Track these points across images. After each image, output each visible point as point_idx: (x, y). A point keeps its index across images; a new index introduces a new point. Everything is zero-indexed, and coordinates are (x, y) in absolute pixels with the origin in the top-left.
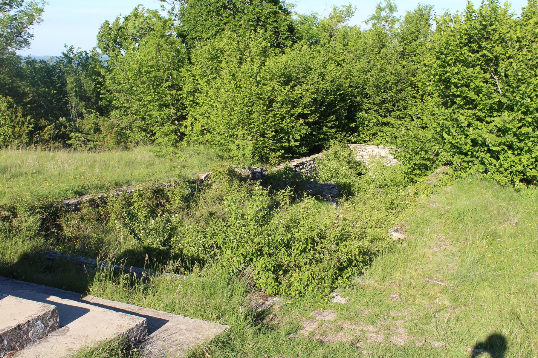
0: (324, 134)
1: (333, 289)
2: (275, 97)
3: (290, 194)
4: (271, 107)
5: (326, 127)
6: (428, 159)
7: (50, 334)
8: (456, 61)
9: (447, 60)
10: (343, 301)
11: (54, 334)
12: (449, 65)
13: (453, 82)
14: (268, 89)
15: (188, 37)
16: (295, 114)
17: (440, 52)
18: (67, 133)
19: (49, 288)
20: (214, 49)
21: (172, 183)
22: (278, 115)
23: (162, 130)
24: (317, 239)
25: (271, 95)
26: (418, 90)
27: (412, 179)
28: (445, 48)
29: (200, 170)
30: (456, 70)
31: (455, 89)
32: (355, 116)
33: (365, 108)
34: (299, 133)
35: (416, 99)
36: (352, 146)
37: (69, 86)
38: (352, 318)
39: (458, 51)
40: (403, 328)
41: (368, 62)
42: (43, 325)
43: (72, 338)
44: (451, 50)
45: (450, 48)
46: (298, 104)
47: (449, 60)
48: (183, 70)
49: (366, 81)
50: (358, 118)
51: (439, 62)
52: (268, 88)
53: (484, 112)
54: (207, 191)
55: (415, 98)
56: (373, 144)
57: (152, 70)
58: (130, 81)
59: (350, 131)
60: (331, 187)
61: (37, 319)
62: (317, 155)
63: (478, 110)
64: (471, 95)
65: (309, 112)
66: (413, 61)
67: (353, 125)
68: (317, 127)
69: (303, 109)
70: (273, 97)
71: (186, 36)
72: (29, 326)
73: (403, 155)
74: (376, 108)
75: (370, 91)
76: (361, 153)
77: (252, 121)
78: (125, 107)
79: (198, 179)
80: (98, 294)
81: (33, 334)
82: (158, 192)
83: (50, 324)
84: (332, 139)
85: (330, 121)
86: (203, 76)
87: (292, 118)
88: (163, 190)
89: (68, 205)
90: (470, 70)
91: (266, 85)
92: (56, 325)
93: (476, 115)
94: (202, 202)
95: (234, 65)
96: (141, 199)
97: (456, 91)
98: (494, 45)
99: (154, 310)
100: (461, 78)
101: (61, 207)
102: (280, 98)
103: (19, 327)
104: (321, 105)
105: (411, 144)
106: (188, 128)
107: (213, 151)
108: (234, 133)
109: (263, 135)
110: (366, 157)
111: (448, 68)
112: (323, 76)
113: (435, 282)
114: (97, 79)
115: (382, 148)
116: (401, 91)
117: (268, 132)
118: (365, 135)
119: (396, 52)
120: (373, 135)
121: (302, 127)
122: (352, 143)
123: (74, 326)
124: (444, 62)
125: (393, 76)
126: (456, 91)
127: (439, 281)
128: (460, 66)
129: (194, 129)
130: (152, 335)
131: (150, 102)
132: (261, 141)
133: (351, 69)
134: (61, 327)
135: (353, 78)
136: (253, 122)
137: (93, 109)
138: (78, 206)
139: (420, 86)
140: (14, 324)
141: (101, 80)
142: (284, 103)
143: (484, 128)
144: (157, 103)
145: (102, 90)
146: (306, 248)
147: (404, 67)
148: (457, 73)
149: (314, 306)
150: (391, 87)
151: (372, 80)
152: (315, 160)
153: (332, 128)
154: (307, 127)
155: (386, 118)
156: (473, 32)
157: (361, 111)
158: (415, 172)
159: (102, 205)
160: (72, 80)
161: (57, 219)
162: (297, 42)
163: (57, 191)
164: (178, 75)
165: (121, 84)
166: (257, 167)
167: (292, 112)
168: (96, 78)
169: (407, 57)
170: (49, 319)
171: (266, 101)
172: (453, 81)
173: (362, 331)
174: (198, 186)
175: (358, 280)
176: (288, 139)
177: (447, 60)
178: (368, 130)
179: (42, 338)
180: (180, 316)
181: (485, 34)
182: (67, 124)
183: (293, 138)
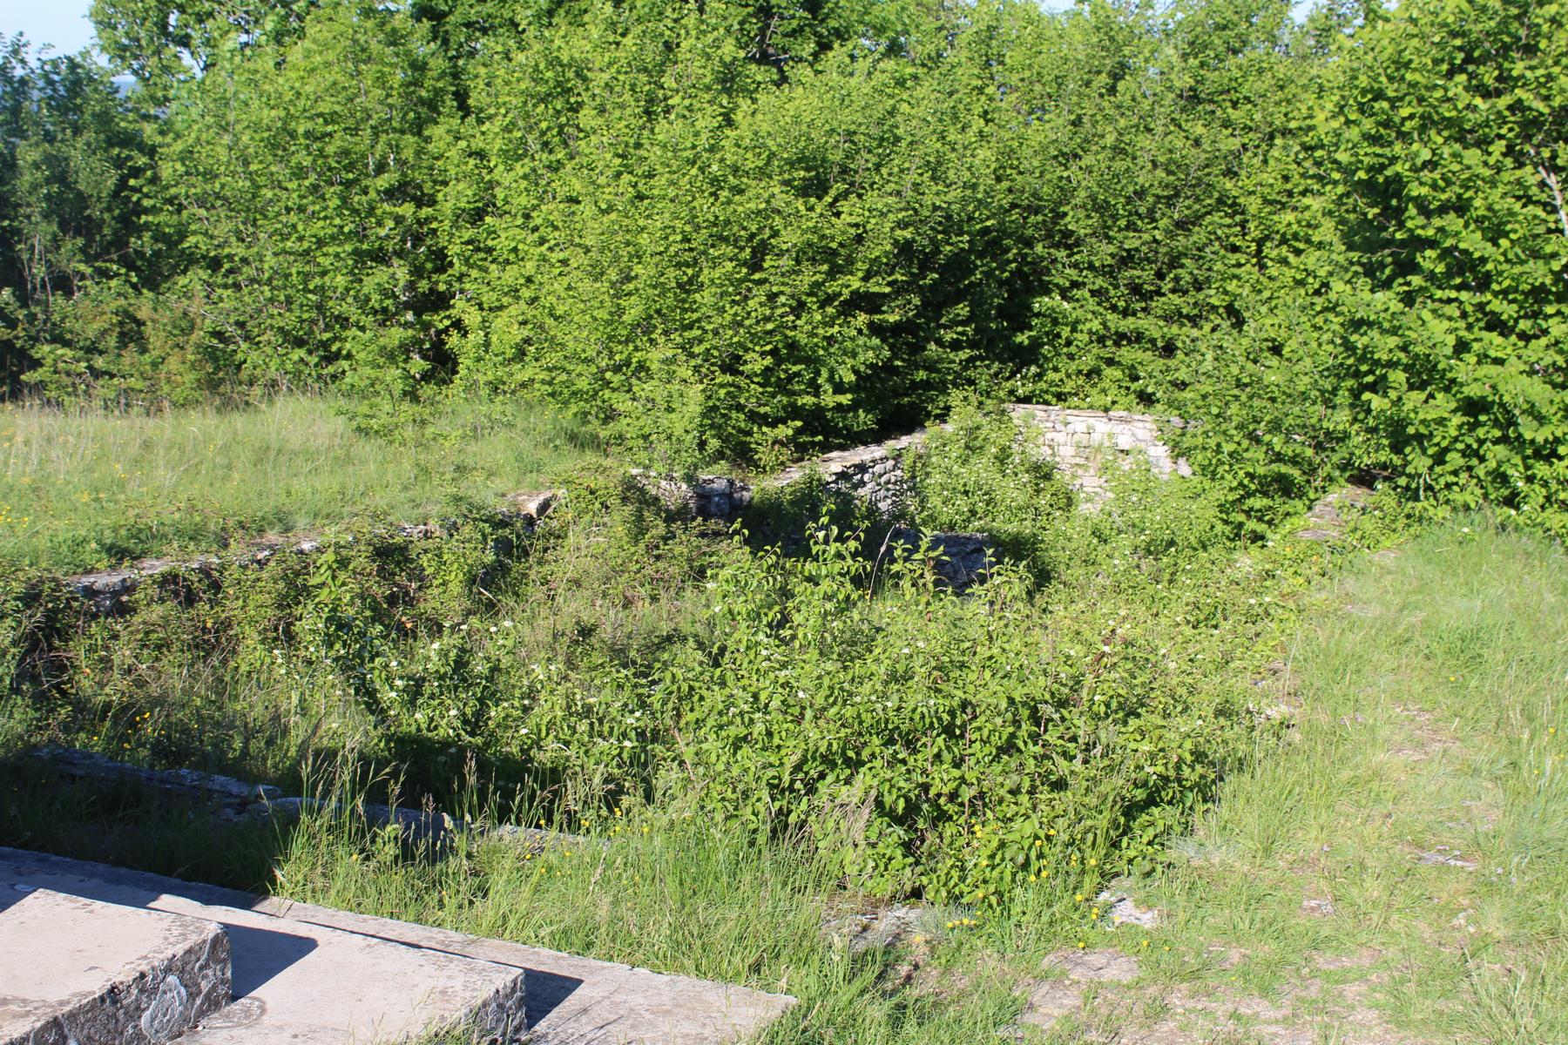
0: (931, 367)
1: (1107, 876)
2: (775, 234)
3: (932, 554)
4: (761, 269)
5: (939, 342)
6: (1294, 461)
7: (204, 1022)
8: (1427, 123)
9: (1397, 120)
10: (1148, 920)
11: (215, 1020)
12: (1403, 136)
13: (1415, 193)
14: (752, 206)
15: (451, 18)
16: (840, 294)
17: (1372, 90)
18: (19, 344)
19: (123, 870)
20: (555, 62)
21: (433, 525)
22: (782, 299)
23: (382, 341)
24: (1047, 710)
25: (760, 229)
26: (1243, 225)
27: (1241, 525)
28: (1391, 79)
29: (519, 482)
30: (1426, 155)
31: (1421, 220)
32: (1030, 309)
33: (1060, 281)
34: (850, 362)
35: (1238, 255)
36: (1019, 412)
37: (26, 179)
38: (1195, 975)
39: (1435, 87)
40: (1370, 1008)
41: (1073, 124)
42: (183, 990)
43: (287, 1034)
44: (1413, 85)
45: (1409, 76)
46: (850, 261)
47: (1404, 119)
48: (437, 132)
49: (1065, 192)
50: (1038, 315)
51: (1368, 125)
52: (748, 205)
53: (1514, 301)
54: (550, 556)
55: (1235, 249)
56: (1091, 407)
57: (329, 128)
58: (253, 167)
59: (1011, 359)
60: (971, 547)
61: (168, 970)
62: (905, 441)
63: (1496, 294)
64: (1473, 242)
65: (887, 290)
66: (1226, 124)
67: (1022, 338)
68: (907, 344)
69: (866, 279)
70: (767, 232)
71: (444, 15)
72: (142, 991)
73: (1212, 443)
74: (1100, 282)
75: (1077, 222)
76: (1049, 436)
77: (695, 316)
78: (230, 257)
79: (518, 515)
80: (309, 892)
81: (153, 1020)
82: (390, 555)
83: (205, 986)
84: (956, 386)
85: (954, 323)
86: (515, 154)
87: (830, 310)
88: (403, 549)
89: (90, 592)
90: (1473, 156)
91: (741, 192)
92: (222, 990)
93: (1488, 309)
94: (535, 593)
95: (626, 119)
96: (342, 576)
97: (1423, 227)
98: (1556, 70)
99: (519, 945)
100: (1441, 183)
101: (68, 600)
102: (790, 238)
103: (113, 993)
104: (926, 263)
105: (1234, 408)
106: (471, 337)
107: (551, 417)
108: (629, 357)
109: (732, 365)
110: (1066, 452)
111: (1398, 148)
112: (935, 170)
113: (1441, 859)
114: (129, 158)
115: (1121, 420)
116: (1182, 225)
117: (748, 357)
118: (1062, 375)
119: (1170, 89)
120: (1089, 375)
121: (861, 341)
122: (1020, 400)
123: (273, 991)
124: (1387, 124)
125: (1160, 173)
126: (1423, 227)
127: (1456, 858)
128: (1440, 140)
129: (494, 338)
130: (541, 1027)
131: (320, 243)
132: (722, 386)
133: (1015, 144)
134: (234, 998)
135: (1019, 178)
136: (699, 320)
137: (111, 261)
138: (125, 598)
139: (1252, 209)
140: (96, 986)
141: (142, 160)
142: (804, 255)
143: (1513, 359)
144: (349, 248)
145: (147, 196)
146: (1013, 736)
147: (1197, 143)
148: (1431, 165)
149: (1049, 934)
150: (1151, 211)
151: (1085, 185)
152: (900, 456)
153: (956, 346)
154: (876, 341)
155: (1131, 319)
156: (1480, 27)
157: (1047, 292)
158: (1250, 502)
159: (205, 597)
160: (34, 155)
161: (57, 643)
162: (831, 48)
163: (43, 543)
164: (419, 153)
165: (216, 176)
166: (717, 476)
167: (833, 287)
168: (125, 153)
169: (1209, 107)
170: (201, 968)
171: (742, 249)
172: (1415, 190)
173: (1235, 1016)
174: (518, 536)
175: (1181, 851)
176: (813, 381)
177: (1397, 120)
178: (1071, 357)
179: (180, 1035)
180: (615, 964)
181: (1522, 32)
182: (21, 314)
183: (831, 379)
